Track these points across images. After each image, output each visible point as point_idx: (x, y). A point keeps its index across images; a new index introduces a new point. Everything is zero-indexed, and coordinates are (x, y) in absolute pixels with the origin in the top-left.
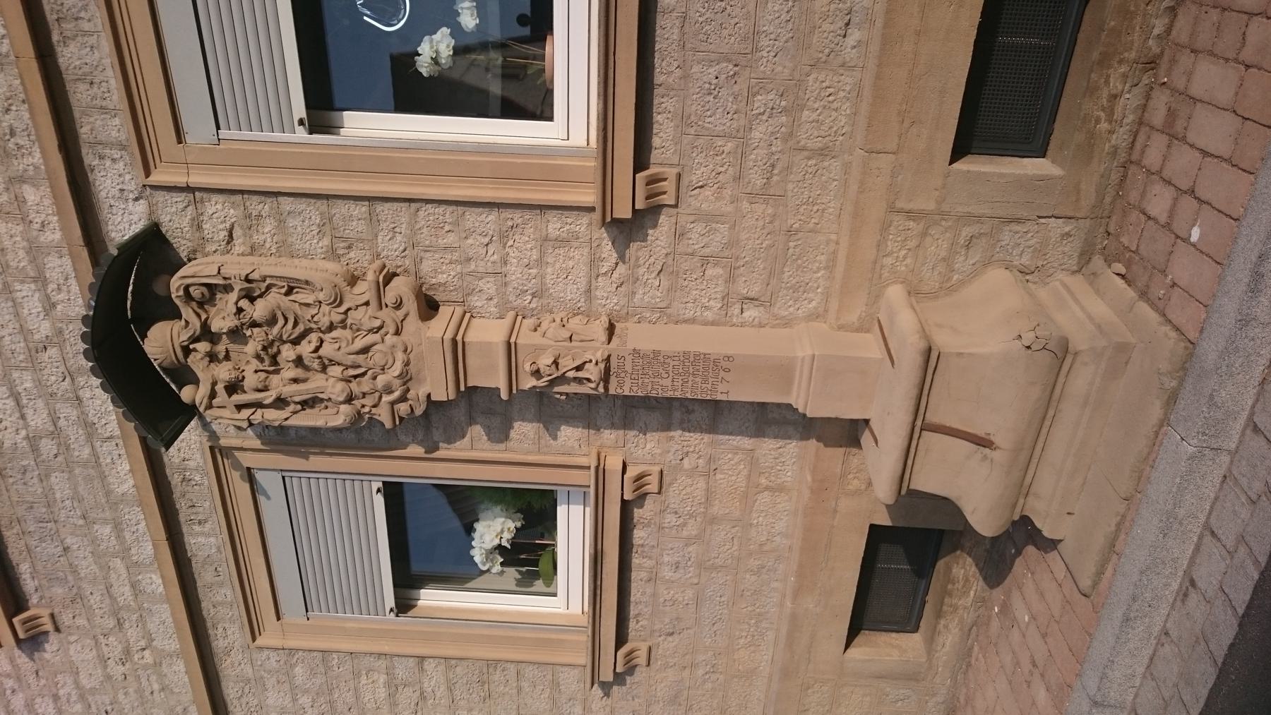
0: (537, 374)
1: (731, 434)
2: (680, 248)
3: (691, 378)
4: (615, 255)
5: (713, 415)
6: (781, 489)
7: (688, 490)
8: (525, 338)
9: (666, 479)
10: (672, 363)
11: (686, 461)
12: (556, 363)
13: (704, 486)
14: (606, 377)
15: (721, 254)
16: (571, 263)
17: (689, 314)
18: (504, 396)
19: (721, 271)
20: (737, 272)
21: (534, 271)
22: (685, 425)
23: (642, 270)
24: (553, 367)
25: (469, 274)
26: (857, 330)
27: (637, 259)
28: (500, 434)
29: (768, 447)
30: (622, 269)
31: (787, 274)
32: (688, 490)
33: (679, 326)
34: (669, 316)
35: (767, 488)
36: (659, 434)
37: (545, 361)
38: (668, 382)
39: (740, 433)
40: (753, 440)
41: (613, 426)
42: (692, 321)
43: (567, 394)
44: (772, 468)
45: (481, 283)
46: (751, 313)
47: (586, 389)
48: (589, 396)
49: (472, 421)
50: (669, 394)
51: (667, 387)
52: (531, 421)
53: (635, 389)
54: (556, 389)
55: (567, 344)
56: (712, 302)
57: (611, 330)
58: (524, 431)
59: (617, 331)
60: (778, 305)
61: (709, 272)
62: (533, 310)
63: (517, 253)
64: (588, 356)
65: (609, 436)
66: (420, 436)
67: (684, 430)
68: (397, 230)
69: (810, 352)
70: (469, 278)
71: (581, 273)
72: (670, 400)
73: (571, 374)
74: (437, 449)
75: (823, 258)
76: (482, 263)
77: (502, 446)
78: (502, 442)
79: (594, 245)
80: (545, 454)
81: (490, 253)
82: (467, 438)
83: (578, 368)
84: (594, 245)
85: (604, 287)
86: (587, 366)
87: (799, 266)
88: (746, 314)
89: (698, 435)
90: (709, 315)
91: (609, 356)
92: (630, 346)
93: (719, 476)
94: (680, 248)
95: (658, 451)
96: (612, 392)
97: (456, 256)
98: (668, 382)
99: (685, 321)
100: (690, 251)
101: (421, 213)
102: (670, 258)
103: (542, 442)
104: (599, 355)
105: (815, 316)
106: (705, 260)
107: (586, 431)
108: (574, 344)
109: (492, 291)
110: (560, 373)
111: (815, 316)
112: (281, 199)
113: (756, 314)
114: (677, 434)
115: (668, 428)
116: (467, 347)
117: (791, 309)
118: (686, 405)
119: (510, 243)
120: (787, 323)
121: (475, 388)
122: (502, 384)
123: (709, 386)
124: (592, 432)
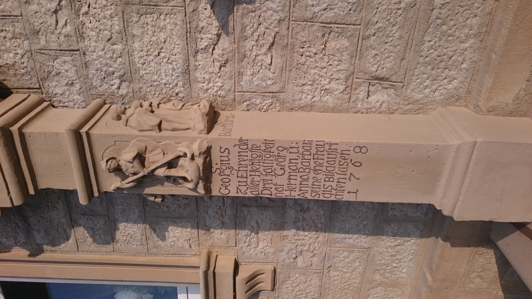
0: (118, 170)
1: (348, 232)
2: (297, 13)
3: (312, 175)
4: (216, 23)
5: (331, 215)
6: (395, 284)
7: (302, 286)
8: (104, 129)
9: (280, 277)
10: (289, 156)
11: (300, 260)
12: (140, 158)
13: (318, 283)
14: (206, 174)
15: (349, 20)
16: (162, 36)
17: (306, 99)
18: (83, 200)
19: (345, 42)
20: (367, 43)
21: (118, 47)
22: (299, 224)
23: (249, 44)
24: (136, 163)
25: (41, 51)
26: (511, 114)
27: (244, 28)
28: (106, 235)
29: (386, 245)
30: (225, 43)
31: (427, 44)
32: (302, 286)
33: (294, 114)
34: (283, 103)
35: (380, 284)
36: (272, 232)
37: (126, 157)
38: (283, 180)
39: (358, 232)
40: (370, 238)
41: (223, 226)
42: (310, 107)
43: (163, 197)
44: (388, 265)
45: (56, 64)
46: (380, 97)
47: (185, 190)
48: (186, 197)
49: (74, 224)
50: (285, 194)
51: (281, 185)
52: (135, 222)
53: (243, 189)
54: (148, 191)
55: (155, 133)
56: (333, 85)
57: (212, 118)
58: (130, 232)
59: (221, 119)
60: (413, 85)
61: (332, 45)
62: (123, 97)
63: (95, 24)
64: (181, 149)
65: (219, 236)
66: (22, 239)
67: (298, 229)
69: (469, 139)
70: (40, 58)
71: (177, 46)
72: (284, 201)
73: (161, 172)
74: (42, 251)
75: (474, 21)
76: (54, 37)
77: (109, 247)
78: (108, 243)
79: (189, 9)
80: (155, 254)
81: (61, 23)
82: (71, 241)
83: (171, 164)
84: (189, 9)
85: (205, 66)
86: (181, 161)
87: (443, 34)
88: (372, 98)
89: (313, 234)
90: (329, 100)
91: (209, 149)
92: (236, 135)
93: (332, 273)
94: (297, 13)
95: (271, 250)
96: (215, 192)
97: (18, 28)
98: (283, 180)
99: (302, 108)
100: (309, 15)
102: (284, 26)
103: (151, 243)
104: (195, 148)
105: (453, 99)
106: (328, 28)
107: (195, 231)
108: (163, 133)
109: (72, 74)
110: (145, 172)
111: (453, 99)
113: (385, 98)
114: (291, 233)
115: (281, 227)
116: (29, 140)
117: (427, 91)
118: (301, 206)
119: (85, 9)
120: (421, 107)
121: (49, 191)
122: (74, 181)
123: (334, 185)
124: (202, 232)
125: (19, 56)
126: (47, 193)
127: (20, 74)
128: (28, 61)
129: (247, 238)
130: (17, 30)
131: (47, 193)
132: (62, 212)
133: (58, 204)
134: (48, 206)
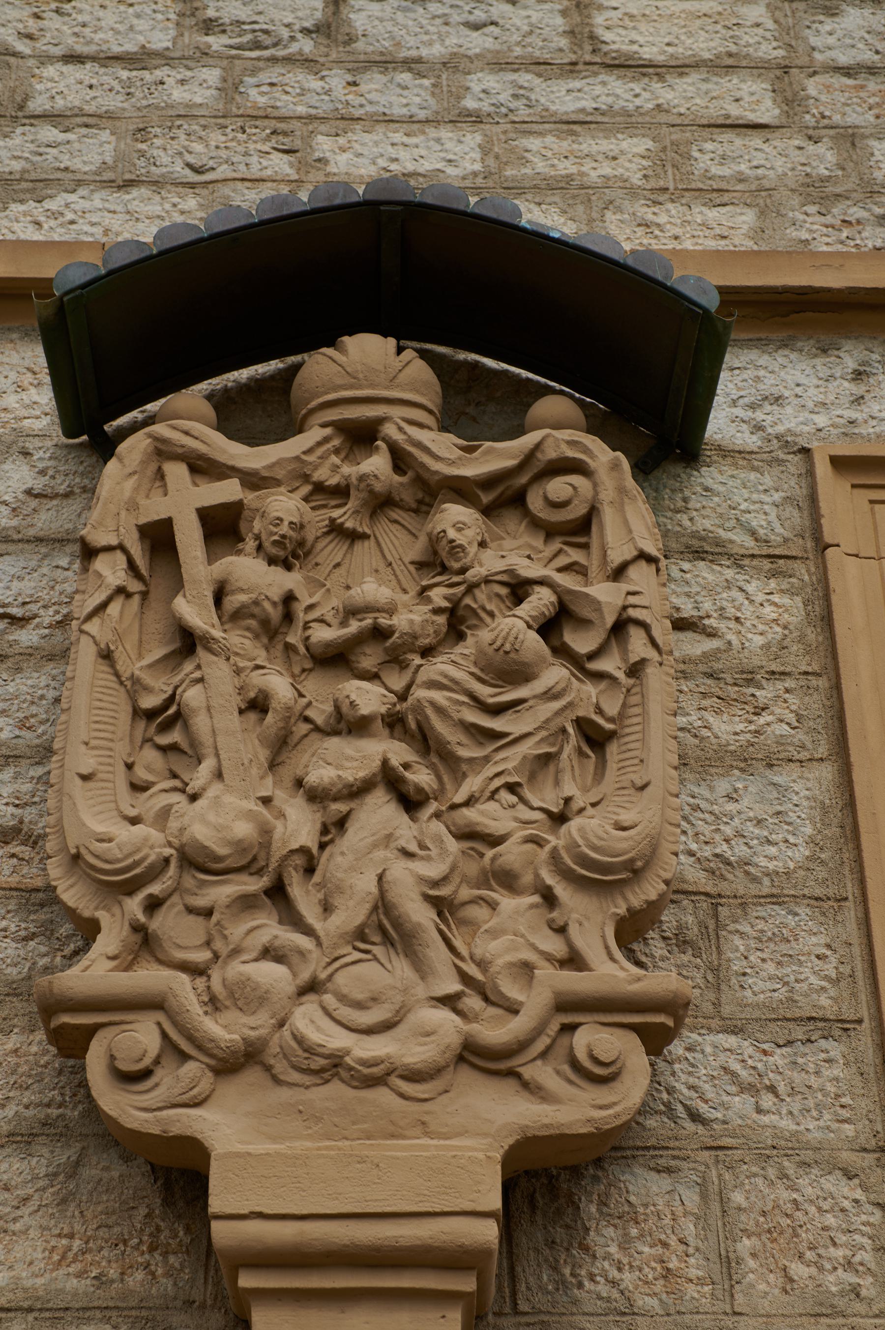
68: (768, 1100)
101: (847, 1191)
112: (827, 772)
125: (614, 1273)
126: (125, 1242)
127: (557, 1261)
128: (600, 1298)
129: (378, 914)
130: (691, 1291)
131: (125, 1242)
132: (40, 1281)
133: (79, 1275)
134: (71, 1236)
